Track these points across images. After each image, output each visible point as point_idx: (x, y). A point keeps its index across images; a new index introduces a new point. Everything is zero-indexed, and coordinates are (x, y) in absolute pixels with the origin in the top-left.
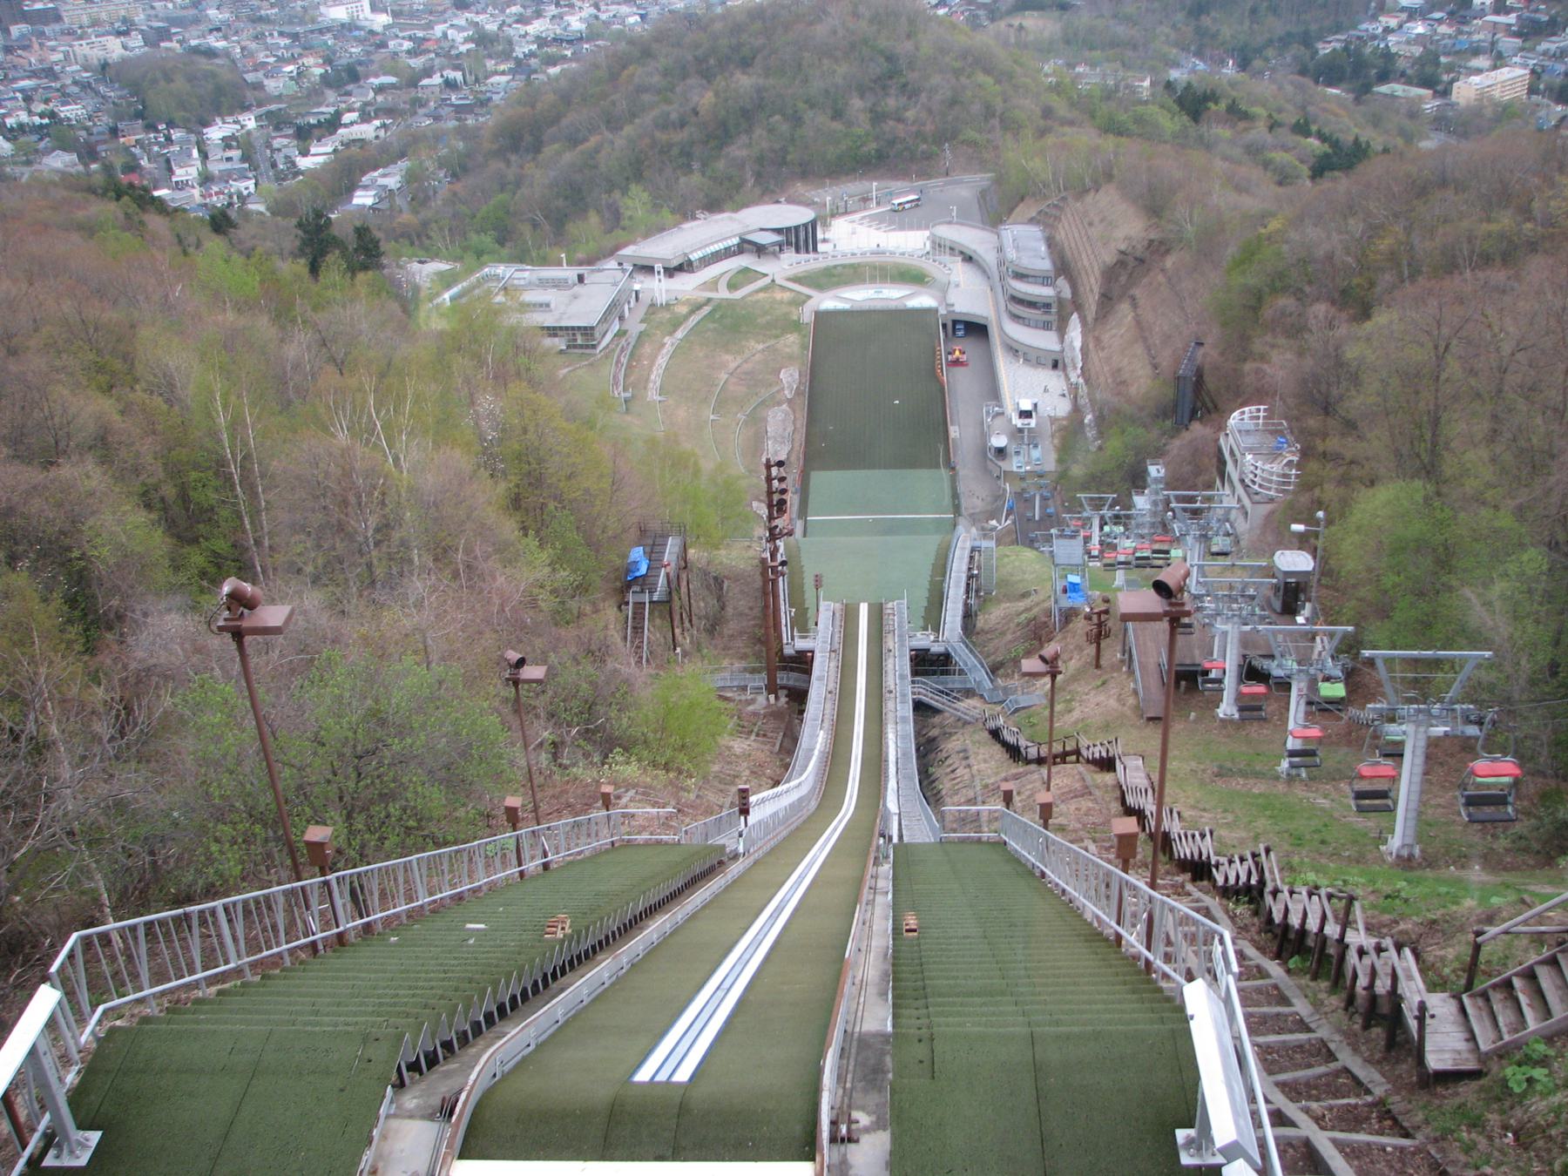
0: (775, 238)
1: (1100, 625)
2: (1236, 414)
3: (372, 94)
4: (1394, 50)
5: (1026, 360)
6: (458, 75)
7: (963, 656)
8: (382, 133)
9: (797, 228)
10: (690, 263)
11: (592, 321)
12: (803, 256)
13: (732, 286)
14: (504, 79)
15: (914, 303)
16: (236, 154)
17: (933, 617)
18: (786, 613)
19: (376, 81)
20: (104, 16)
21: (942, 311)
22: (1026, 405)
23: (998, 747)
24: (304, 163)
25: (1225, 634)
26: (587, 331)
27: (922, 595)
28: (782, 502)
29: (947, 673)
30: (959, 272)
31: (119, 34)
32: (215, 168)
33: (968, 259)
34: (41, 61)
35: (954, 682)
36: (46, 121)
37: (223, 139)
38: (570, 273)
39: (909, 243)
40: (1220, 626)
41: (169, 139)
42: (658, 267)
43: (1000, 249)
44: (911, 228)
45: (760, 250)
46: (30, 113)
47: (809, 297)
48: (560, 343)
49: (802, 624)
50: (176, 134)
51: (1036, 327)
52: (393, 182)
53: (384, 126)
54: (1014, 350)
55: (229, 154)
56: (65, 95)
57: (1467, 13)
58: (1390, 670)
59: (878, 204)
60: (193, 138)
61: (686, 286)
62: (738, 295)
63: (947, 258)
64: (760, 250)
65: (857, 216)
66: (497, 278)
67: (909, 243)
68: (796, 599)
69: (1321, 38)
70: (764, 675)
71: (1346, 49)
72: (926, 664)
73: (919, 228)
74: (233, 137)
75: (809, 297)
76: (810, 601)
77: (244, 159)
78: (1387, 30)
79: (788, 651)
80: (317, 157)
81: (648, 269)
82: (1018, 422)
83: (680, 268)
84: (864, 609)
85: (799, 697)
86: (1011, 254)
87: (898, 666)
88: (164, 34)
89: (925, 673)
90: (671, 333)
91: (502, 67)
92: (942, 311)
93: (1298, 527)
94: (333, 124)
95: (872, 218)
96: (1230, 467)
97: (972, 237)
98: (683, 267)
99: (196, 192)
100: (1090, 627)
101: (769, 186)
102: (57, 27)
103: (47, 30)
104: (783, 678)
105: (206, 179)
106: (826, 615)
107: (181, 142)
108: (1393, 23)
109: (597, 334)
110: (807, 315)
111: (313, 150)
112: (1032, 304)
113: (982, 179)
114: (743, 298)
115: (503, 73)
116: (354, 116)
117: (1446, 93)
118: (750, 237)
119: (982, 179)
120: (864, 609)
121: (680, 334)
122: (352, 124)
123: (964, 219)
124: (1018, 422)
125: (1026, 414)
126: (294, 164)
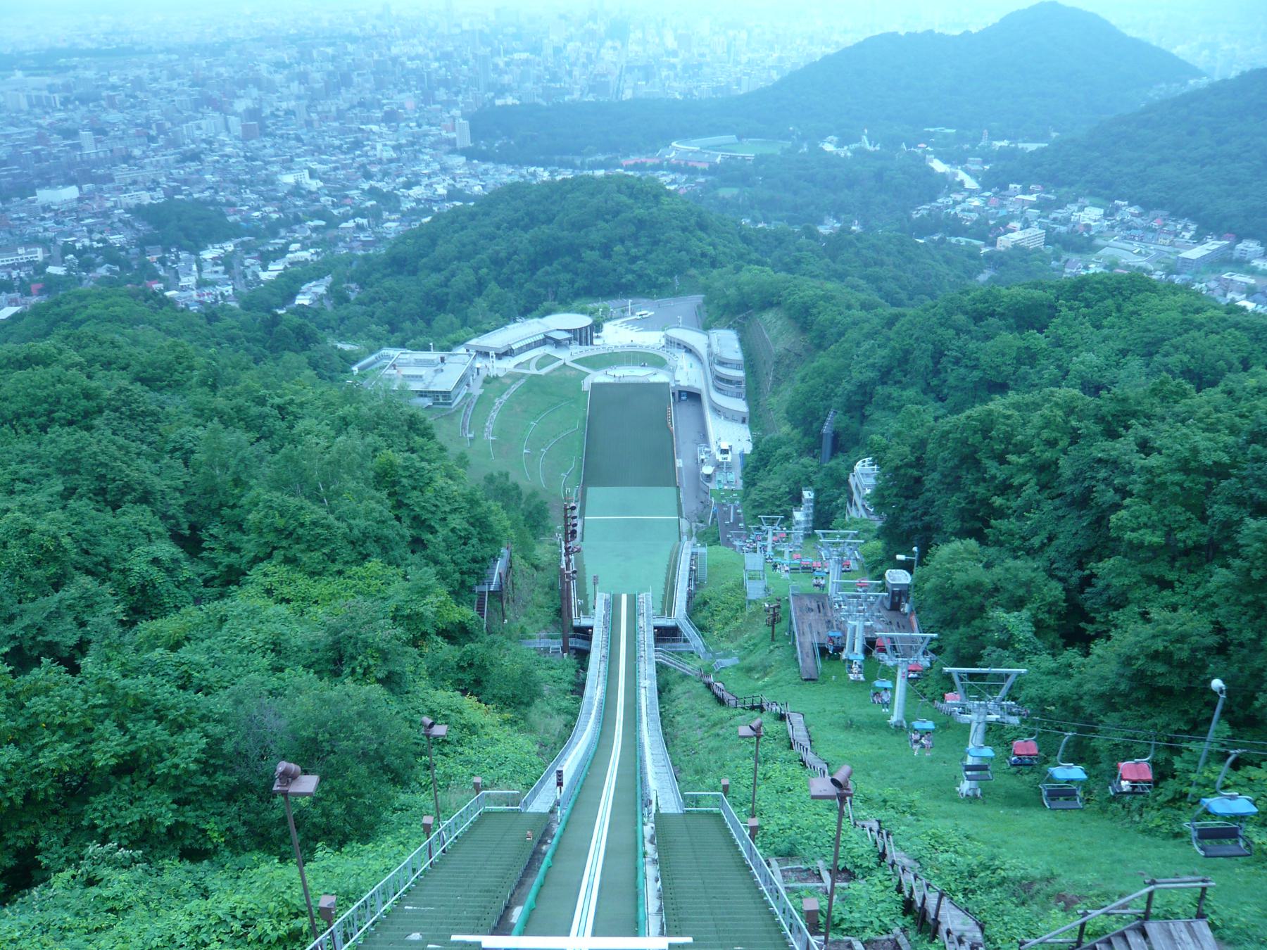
1: (774, 615)
2: (860, 462)
3: (309, 232)
4: (960, 215)
5: (726, 418)
6: (365, 221)
7: (688, 629)
8: (315, 258)
11: (449, 387)
12: (585, 347)
13: (540, 366)
14: (393, 225)
15: (653, 379)
16: (221, 268)
17: (667, 608)
18: (575, 602)
20: (140, 179)
21: (673, 385)
22: (725, 446)
23: (709, 695)
24: (264, 276)
25: (855, 627)
26: (446, 394)
27: (660, 586)
28: (574, 532)
29: (674, 641)
30: (683, 360)
31: (149, 189)
32: (207, 276)
33: (689, 350)
34: (99, 207)
35: (681, 646)
36: (101, 245)
37: (213, 259)
38: (434, 355)
39: (652, 339)
40: (851, 623)
41: (177, 256)
42: (492, 353)
43: (709, 346)
44: (653, 330)
45: (558, 343)
46: (91, 240)
48: (428, 402)
49: (584, 609)
50: (183, 255)
51: (734, 420)
52: (321, 290)
53: (317, 253)
54: (717, 410)
56: (113, 228)
57: (1006, 193)
58: (961, 679)
60: (193, 257)
61: (508, 364)
62: (543, 372)
63: (675, 350)
64: (558, 343)
65: (618, 322)
66: (388, 357)
67: (652, 339)
68: (582, 594)
69: (913, 208)
71: (929, 215)
72: (665, 635)
73: (658, 330)
74: (219, 258)
76: (590, 590)
77: (225, 273)
78: (956, 203)
79: (576, 623)
80: (273, 271)
81: (486, 355)
82: (720, 457)
84: (624, 598)
85: (582, 656)
86: (716, 349)
87: (647, 637)
88: (177, 190)
89: (664, 641)
90: (500, 397)
91: (393, 217)
92: (673, 385)
93: (900, 557)
94: (284, 251)
95: (628, 322)
96: (856, 496)
97: (695, 338)
98: (508, 353)
99: (194, 293)
100: (769, 617)
101: (565, 302)
102: (111, 185)
103: (104, 187)
104: (573, 643)
105: (201, 284)
106: (600, 610)
107: (186, 261)
108: (959, 198)
109: (452, 396)
111: (271, 267)
112: (729, 382)
113: (698, 298)
114: (547, 375)
115: (394, 221)
116: (297, 246)
117: (993, 244)
118: (551, 335)
119: (698, 298)
120: (624, 598)
121: (505, 397)
123: (687, 325)
124: (720, 457)
125: (724, 452)
126: (258, 276)
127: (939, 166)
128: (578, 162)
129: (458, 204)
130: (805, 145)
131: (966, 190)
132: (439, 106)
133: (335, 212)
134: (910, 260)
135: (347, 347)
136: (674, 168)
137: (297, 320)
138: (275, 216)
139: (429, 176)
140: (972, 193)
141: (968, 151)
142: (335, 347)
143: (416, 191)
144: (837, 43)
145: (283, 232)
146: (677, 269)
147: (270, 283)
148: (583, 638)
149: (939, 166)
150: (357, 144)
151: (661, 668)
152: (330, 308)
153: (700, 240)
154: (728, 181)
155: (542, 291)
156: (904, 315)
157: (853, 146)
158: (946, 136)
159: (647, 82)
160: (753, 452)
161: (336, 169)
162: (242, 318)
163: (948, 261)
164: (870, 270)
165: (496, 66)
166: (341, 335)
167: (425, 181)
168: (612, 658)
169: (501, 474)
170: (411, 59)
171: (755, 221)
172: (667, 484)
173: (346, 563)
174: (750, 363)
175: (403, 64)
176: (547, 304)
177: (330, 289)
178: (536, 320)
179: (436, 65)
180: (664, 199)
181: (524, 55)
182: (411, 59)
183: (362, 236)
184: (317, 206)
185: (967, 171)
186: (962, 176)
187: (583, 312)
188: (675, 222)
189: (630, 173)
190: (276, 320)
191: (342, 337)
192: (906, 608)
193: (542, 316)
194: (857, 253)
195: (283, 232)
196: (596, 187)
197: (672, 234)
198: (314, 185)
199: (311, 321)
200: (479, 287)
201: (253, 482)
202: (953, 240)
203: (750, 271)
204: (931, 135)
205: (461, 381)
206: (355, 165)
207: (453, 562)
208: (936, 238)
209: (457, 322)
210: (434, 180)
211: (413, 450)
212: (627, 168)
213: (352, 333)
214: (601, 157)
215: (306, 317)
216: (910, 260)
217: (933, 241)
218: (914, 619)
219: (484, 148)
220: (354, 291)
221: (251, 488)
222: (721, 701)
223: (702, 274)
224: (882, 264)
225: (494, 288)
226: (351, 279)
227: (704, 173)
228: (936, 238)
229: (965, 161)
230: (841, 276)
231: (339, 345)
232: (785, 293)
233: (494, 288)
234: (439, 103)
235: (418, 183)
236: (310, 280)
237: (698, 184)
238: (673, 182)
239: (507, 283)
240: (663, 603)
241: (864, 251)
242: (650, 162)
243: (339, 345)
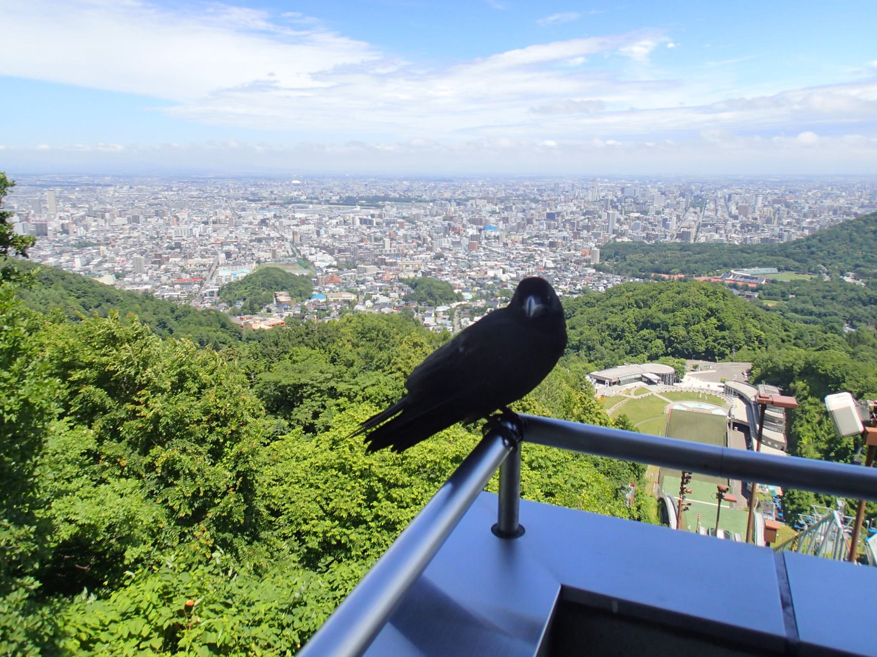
0: (658, 378)
15: (714, 412)
42: (607, 381)
45: (650, 382)
55: (445, 317)
59: (701, 370)
61: (615, 390)
75: (669, 403)
81: (603, 382)
110: (667, 411)
154: (770, 296)
181: (637, 215)
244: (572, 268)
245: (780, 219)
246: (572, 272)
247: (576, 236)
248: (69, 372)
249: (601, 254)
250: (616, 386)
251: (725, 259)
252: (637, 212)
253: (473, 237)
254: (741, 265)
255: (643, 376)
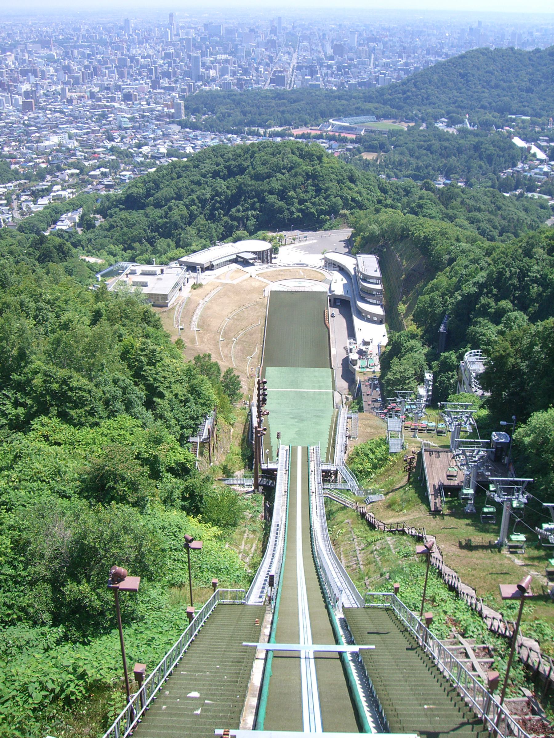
0: (254, 256)
6: (107, 170)
9: (263, 252)
10: (212, 266)
12: (265, 265)
19: (69, 172)
38: (156, 268)
47: (267, 284)
49: (269, 457)
53: (72, 192)
70: (253, 479)
72: (327, 476)
79: (264, 467)
83: (208, 269)
87: (315, 479)
95: (298, 248)
110: (267, 294)
115: (128, 171)
122: (58, 191)
127: (518, 142)
128: (262, 131)
129: (174, 159)
130: (424, 125)
131: (538, 160)
132: (162, 91)
133: (86, 164)
134: (499, 208)
135: (92, 260)
136: (331, 138)
137: (58, 240)
138: (43, 166)
139: (155, 140)
140: (542, 161)
141: (539, 132)
142: (85, 261)
143: (145, 149)
144: (446, 54)
145: (49, 178)
146: (333, 211)
147: (38, 214)
148: (269, 478)
149: (518, 142)
150: (104, 116)
151: (328, 501)
152: (80, 232)
153: (350, 189)
154: (370, 149)
155: (235, 223)
156: (498, 247)
157: (459, 126)
158: (523, 121)
159: (312, 77)
160: (388, 344)
161: (87, 133)
162: (19, 237)
163: (526, 210)
164: (471, 214)
165: (204, 64)
166: (88, 251)
167: (152, 143)
168: (291, 492)
169: (205, 356)
170: (144, 57)
171: (388, 176)
172: (323, 366)
173: (100, 418)
174: (385, 278)
175: (137, 61)
176: (240, 233)
177: (82, 218)
178: (231, 244)
179: (162, 62)
180: (325, 159)
181: (224, 57)
182: (144, 57)
183: (105, 181)
184: (73, 159)
185: (540, 147)
186: (534, 149)
187: (264, 239)
188: (333, 176)
189: (300, 140)
190: (43, 240)
191: (89, 253)
192: (506, 460)
193: (235, 241)
194: (462, 202)
195: (49, 178)
196: (277, 151)
197: (330, 184)
198: (73, 144)
199: (67, 240)
200: (191, 219)
201: (33, 357)
202: (530, 195)
203: (386, 212)
204: (513, 120)
205: (175, 287)
206: (102, 130)
207: (175, 418)
208: (517, 193)
209: (173, 244)
210: (158, 142)
211: (147, 336)
212: (297, 137)
213: (96, 250)
214: (279, 129)
215: (63, 238)
216: (499, 208)
217: (515, 195)
218: (511, 467)
219: (194, 120)
220: (99, 221)
221: (32, 362)
222: (372, 526)
223: (352, 214)
224: (479, 210)
225: (201, 220)
226: (97, 212)
227: (352, 141)
228: (517, 193)
229: (538, 139)
230: (452, 219)
231: (88, 259)
232: (412, 229)
233: (201, 220)
234: (162, 88)
235: (146, 144)
236: (68, 211)
237: (348, 150)
238: (330, 148)
239: (211, 217)
240: (327, 453)
241: (467, 201)
242: (313, 133)
243: (88, 259)
244: (153, 126)
245: (376, 59)
246: (154, 131)
247: (155, 84)
248: (480, 319)
249: (186, 108)
250: (208, 272)
251: (322, 106)
252: (225, 53)
253: (27, 94)
254: (339, 114)
255: (237, 256)
